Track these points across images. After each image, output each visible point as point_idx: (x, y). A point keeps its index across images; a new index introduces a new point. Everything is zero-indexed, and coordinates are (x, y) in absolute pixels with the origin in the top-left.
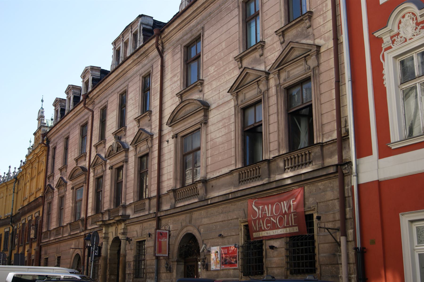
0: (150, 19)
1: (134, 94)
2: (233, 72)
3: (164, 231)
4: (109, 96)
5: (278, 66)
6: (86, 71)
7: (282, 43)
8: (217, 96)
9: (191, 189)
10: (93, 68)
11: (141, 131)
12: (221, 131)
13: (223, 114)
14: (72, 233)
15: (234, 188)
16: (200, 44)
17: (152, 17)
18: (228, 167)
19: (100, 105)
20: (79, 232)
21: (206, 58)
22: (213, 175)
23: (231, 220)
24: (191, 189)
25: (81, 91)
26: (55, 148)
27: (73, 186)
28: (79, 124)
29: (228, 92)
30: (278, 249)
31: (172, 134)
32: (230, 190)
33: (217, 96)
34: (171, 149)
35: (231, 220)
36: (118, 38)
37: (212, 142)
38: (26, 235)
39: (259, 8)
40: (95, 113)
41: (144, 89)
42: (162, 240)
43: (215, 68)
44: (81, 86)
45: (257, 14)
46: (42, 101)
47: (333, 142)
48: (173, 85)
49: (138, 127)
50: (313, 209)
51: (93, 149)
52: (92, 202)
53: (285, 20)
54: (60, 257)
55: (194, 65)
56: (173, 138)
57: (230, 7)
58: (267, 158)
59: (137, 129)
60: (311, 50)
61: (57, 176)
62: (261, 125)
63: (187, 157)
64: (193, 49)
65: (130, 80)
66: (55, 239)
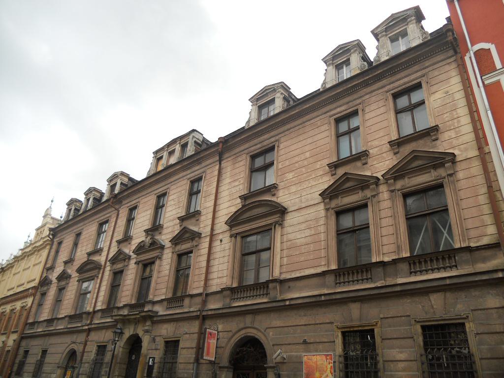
0: (200, 135)
1: (177, 196)
2: (322, 178)
3: (214, 332)
4: (143, 197)
5: (113, 260)
6: (115, 176)
7: (181, 226)
8: (297, 200)
9: (255, 289)
10: (123, 174)
11: (120, 252)
12: (304, 233)
13: (307, 216)
14: (69, 326)
15: (327, 290)
16: (166, 198)
17: (202, 135)
18: (315, 268)
19: (129, 204)
20: (80, 325)
21: (282, 165)
22: (291, 275)
23: (320, 324)
24: (255, 289)
25: (82, 205)
26: (60, 243)
27: (80, 278)
28: (98, 222)
29: (170, 241)
30: (287, 364)
31: (77, 279)
32: (319, 291)
33: (297, 200)
34: (225, 248)
35: (320, 324)
36: (162, 149)
37: (289, 243)
38: (4, 323)
39: (165, 202)
40: (120, 212)
41: (157, 206)
42: (211, 342)
43: (295, 175)
44: (104, 191)
45: (163, 206)
46: (52, 201)
47: (200, 295)
48: (233, 189)
49: (118, 248)
50: (465, 316)
51: (114, 244)
52: (104, 296)
53: (123, 236)
54: (28, 351)
55: (194, 197)
56: (135, 264)
57: (318, 123)
58: (118, 306)
59: (117, 250)
60: (369, 181)
61: (59, 270)
62: (190, 267)
63: (144, 282)
64: (196, 185)
65: (172, 184)
66: (45, 331)
